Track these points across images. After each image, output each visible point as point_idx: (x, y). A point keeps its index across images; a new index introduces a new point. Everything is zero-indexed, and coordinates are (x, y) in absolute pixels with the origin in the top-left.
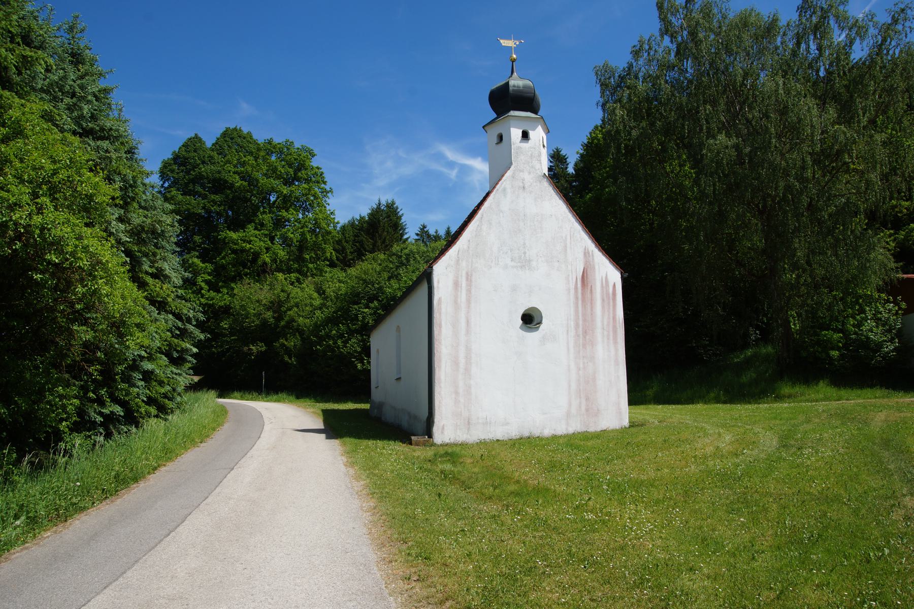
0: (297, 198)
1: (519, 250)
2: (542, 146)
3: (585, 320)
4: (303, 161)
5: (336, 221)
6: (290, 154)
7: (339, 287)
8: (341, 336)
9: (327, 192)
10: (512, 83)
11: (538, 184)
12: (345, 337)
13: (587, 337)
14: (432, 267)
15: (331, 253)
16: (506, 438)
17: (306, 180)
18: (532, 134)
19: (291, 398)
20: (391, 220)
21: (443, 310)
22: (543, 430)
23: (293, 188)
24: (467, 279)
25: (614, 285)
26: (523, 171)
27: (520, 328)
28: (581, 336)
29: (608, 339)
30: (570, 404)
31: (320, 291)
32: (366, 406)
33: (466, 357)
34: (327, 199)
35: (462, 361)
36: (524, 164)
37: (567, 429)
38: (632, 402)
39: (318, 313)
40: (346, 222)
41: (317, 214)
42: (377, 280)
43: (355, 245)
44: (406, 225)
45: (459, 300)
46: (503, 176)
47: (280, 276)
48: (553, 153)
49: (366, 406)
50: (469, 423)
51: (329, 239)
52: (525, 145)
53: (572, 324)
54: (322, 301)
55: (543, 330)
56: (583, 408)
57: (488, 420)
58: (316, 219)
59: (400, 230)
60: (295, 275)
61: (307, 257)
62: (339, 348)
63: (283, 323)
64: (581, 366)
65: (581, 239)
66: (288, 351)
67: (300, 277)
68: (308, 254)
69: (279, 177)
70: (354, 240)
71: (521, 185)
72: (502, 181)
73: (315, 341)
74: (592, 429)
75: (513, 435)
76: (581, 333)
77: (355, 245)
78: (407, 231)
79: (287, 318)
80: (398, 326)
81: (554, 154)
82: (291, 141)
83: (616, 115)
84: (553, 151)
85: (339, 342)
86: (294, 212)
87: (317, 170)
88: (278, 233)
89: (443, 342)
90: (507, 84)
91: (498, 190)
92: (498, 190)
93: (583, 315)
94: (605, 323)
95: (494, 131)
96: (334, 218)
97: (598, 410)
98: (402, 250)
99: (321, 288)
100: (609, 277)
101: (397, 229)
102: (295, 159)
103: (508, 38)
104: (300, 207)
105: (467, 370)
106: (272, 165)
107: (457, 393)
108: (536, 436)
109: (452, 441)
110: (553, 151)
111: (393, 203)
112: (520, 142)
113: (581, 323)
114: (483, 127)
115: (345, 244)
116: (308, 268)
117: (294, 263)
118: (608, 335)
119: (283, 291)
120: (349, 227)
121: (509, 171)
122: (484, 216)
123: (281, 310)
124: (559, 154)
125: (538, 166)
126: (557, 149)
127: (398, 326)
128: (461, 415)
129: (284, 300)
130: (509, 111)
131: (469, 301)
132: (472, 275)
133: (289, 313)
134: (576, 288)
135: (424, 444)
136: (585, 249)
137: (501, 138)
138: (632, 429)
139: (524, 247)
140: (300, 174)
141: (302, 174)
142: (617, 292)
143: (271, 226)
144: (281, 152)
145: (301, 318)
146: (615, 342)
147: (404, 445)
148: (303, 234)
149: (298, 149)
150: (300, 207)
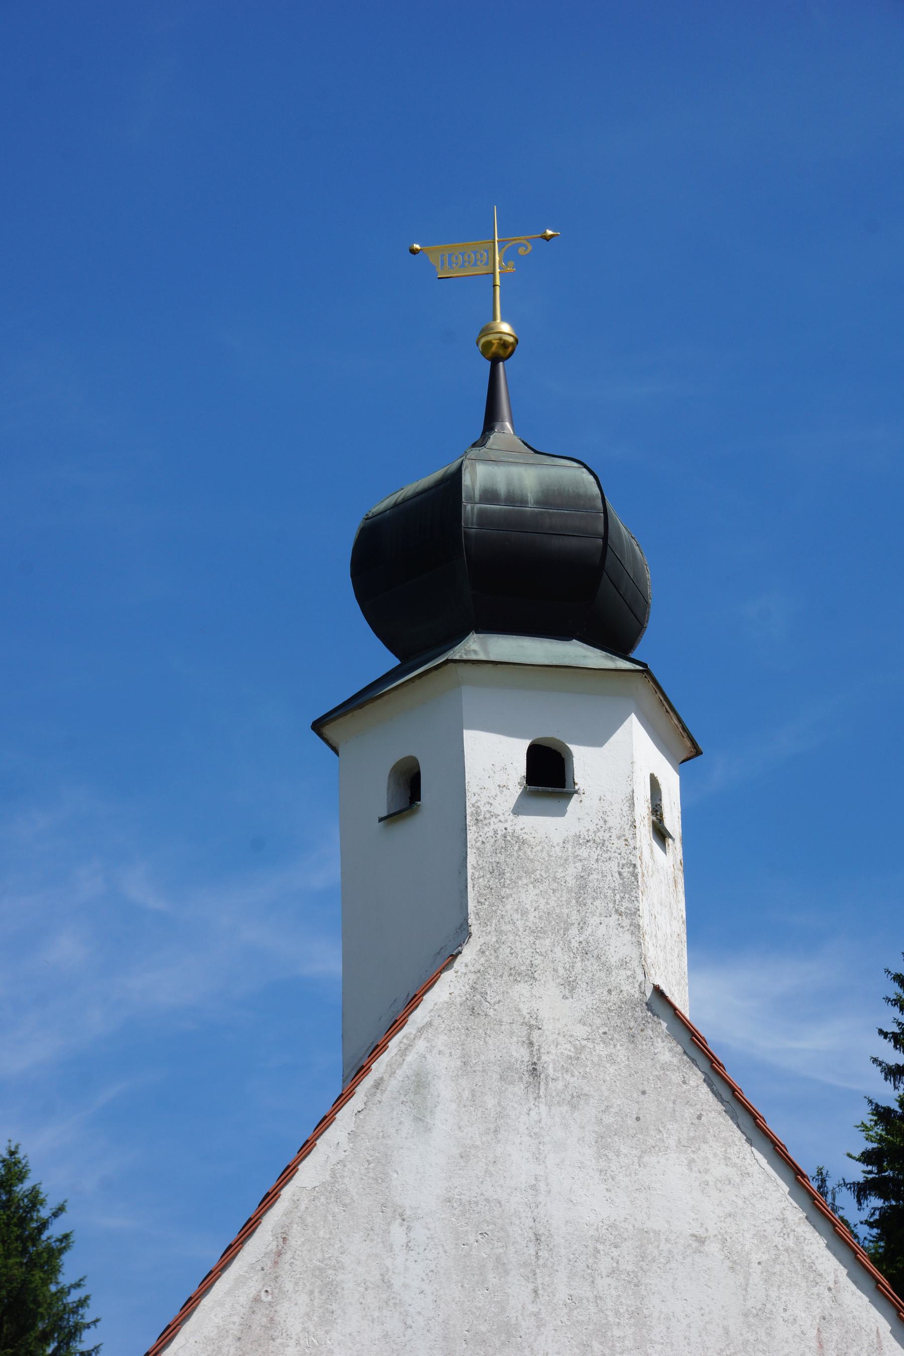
11: (621, 1053)
26: (531, 976)
36: (537, 933)
46: (413, 1002)
72: (408, 1029)
90: (453, 481)
91: (378, 1085)
92: (378, 1085)
103: (550, 230)
114: (318, 726)
121: (447, 976)
122: (295, 1241)
130: (458, 636)
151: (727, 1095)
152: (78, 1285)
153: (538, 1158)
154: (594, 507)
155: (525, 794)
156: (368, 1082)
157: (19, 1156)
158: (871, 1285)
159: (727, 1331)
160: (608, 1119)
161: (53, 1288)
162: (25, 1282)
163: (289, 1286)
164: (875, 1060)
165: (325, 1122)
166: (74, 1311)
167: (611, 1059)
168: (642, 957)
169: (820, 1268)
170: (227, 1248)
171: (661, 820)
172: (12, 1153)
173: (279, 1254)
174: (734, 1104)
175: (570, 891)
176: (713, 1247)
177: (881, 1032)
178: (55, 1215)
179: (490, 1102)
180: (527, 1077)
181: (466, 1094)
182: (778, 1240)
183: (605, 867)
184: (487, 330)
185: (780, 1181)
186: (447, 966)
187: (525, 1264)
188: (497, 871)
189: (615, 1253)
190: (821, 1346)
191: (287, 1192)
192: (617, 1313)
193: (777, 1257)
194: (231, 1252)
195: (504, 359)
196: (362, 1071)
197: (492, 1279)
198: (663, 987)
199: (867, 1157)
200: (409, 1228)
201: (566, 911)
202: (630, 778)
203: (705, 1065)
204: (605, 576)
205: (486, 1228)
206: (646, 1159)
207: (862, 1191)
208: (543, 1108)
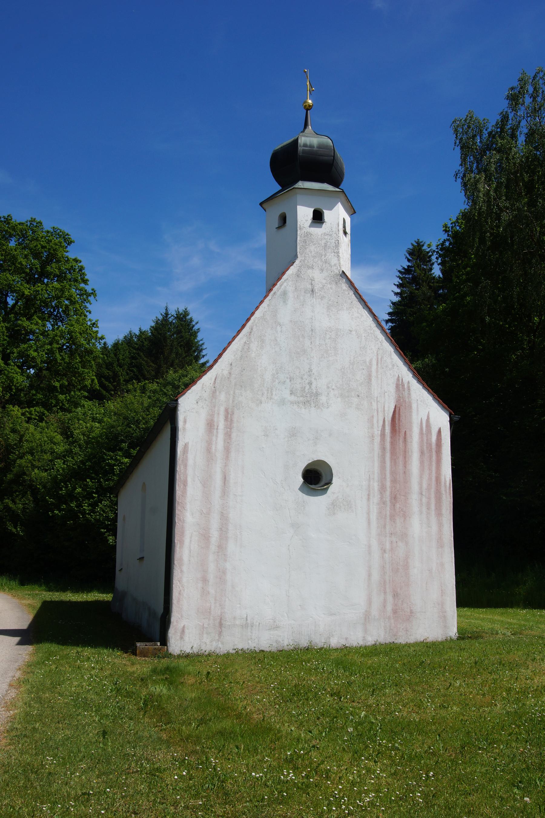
0: (44, 302)
1: (302, 378)
2: (341, 232)
3: (394, 481)
4: (54, 250)
5: (99, 335)
6: (37, 239)
7: (92, 427)
8: (89, 496)
9: (89, 295)
10: (302, 140)
12: (94, 498)
13: (398, 505)
14: (177, 400)
15: (93, 380)
16: (274, 649)
17: (58, 276)
18: (327, 215)
19: (13, 583)
20: (182, 337)
21: (190, 462)
22: (329, 638)
23: (39, 287)
24: (226, 418)
25: (439, 432)
27: (299, 489)
28: (388, 503)
29: (429, 508)
30: (370, 602)
31: (67, 433)
32: (108, 597)
33: (221, 529)
34: (88, 305)
35: (215, 535)
36: (314, 257)
37: (364, 639)
38: (461, 602)
39: (59, 463)
40: (121, 337)
41: (72, 325)
42: (143, 418)
43: (132, 371)
44: (203, 344)
45: (213, 448)
46: (284, 273)
47: (16, 410)
48: (411, 247)
49: (108, 597)
50: (221, 625)
51: (90, 361)
52: (317, 231)
53: (376, 486)
54: (67, 447)
55: (334, 493)
56: (389, 608)
57: (249, 622)
58: (70, 333)
59: (195, 351)
60: (37, 409)
61: (57, 384)
62: (85, 512)
63: (10, 476)
64: (388, 546)
65: (393, 365)
66: (14, 518)
67: (46, 412)
68: (58, 381)
69: (19, 271)
70: (132, 363)
71: (309, 287)
73: (52, 503)
74: (402, 640)
75: (286, 643)
76: (388, 499)
77: (132, 371)
78: (204, 353)
79: (15, 470)
80: (144, 483)
81: (413, 250)
82: (38, 220)
83: (479, 191)
84: (412, 244)
85: (86, 507)
86: (40, 322)
87: (74, 264)
88: (15, 350)
89: (188, 507)
90: (296, 141)
91: (274, 293)
92: (274, 293)
93: (393, 473)
94: (425, 486)
95: (275, 211)
96: (97, 332)
97: (411, 612)
98: (180, 378)
99: (68, 428)
100: (432, 420)
101: (190, 349)
102: (43, 247)
104: (50, 314)
105: (221, 548)
106: (10, 254)
107: (205, 580)
108: (319, 647)
109: (195, 650)
110: (412, 244)
111: (186, 313)
112: (310, 226)
113: (388, 484)
115: (117, 369)
116: (58, 400)
117: (37, 392)
118: (428, 504)
119: (14, 431)
120: (125, 345)
121: (292, 267)
122: (254, 329)
123: (9, 458)
124: (420, 249)
125: (334, 261)
126: (418, 243)
127: (144, 483)
128: (210, 612)
129: (15, 444)
130: (296, 182)
131: (227, 450)
132: (233, 413)
133: (18, 461)
134: (383, 435)
135: (155, 654)
136: (398, 379)
137: (283, 219)
138: (462, 643)
139: (310, 376)
140: (49, 268)
141: (53, 268)
142: (443, 442)
143: (5, 340)
144: (24, 236)
145: (36, 471)
146: (439, 514)
147: (125, 655)
148: (51, 352)
149: (48, 232)
150: (50, 314)
151: (358, 297)
152: (202, 340)
153: (313, 311)
154: (331, 149)
155: (312, 222)
156: (272, 293)
157: (187, 310)
158: (390, 341)
159: (356, 351)
160: (330, 303)
161: (196, 341)
162: (189, 339)
163: (253, 340)
164: (392, 291)
165: (262, 302)
166: (201, 346)
167: (331, 288)
168: (340, 263)
169: (378, 337)
170: (441, 439)
171: (345, 230)
172: (186, 309)
173: (251, 333)
174: (360, 299)
175: (322, 247)
176: (354, 333)
177: (394, 284)
178: (196, 324)
179: (302, 298)
180: (311, 292)
181: (296, 296)
182: (369, 331)
183: (331, 241)
184: (305, 102)
185: (370, 317)
186: (292, 265)
187: (309, 336)
188: (305, 242)
189: (330, 334)
190: (377, 355)
191: (252, 318)
192: (330, 348)
193: (369, 335)
194: (239, 332)
195: (309, 110)
196: (271, 290)
197: (301, 339)
198: (344, 271)
199: (389, 314)
200: (281, 327)
201: (321, 252)
202: (338, 218)
203: (354, 290)
204: (333, 167)
205: (300, 328)
206: (338, 312)
207: (387, 321)
208: (314, 300)
